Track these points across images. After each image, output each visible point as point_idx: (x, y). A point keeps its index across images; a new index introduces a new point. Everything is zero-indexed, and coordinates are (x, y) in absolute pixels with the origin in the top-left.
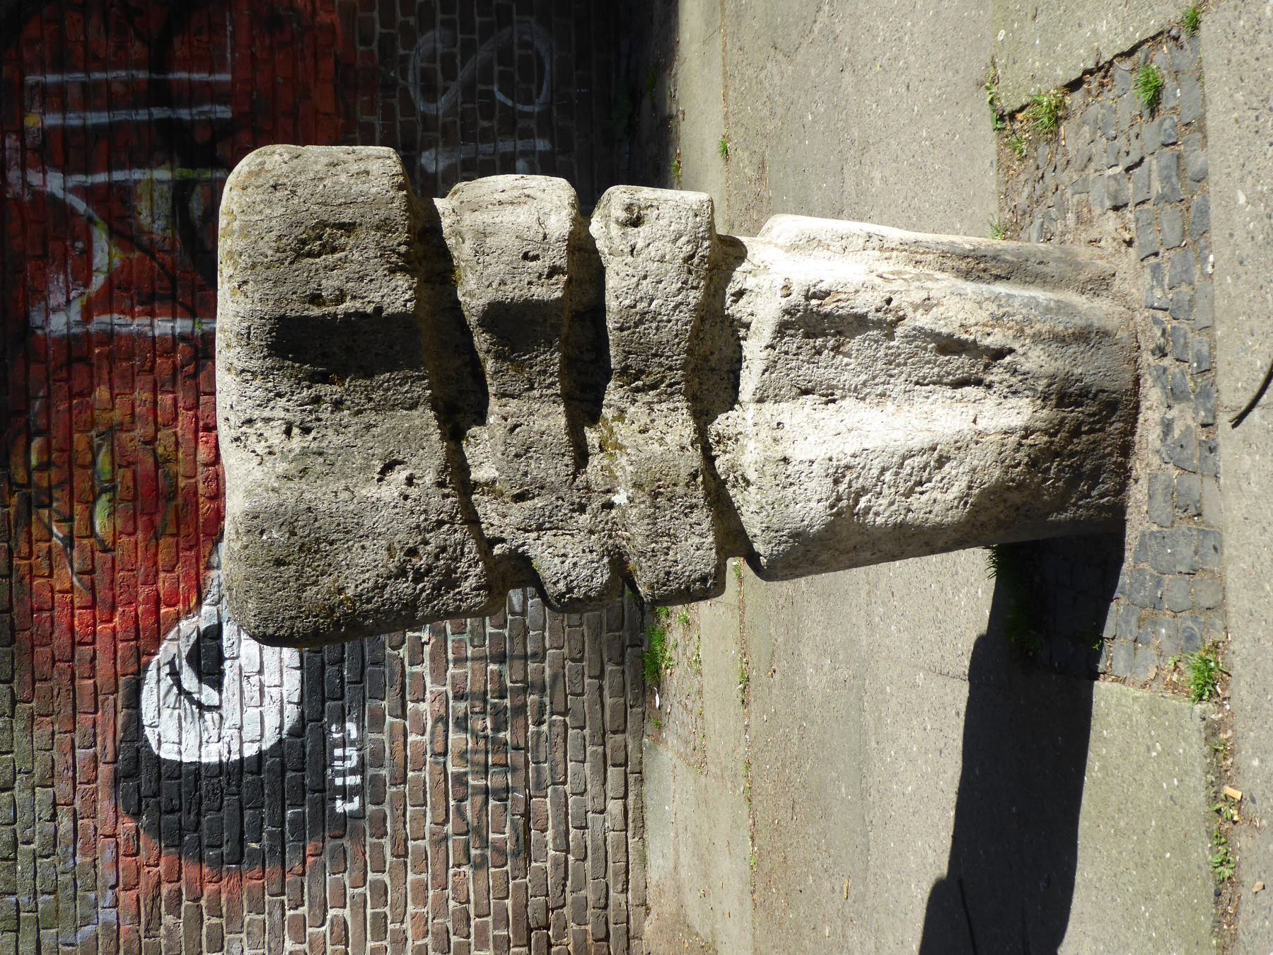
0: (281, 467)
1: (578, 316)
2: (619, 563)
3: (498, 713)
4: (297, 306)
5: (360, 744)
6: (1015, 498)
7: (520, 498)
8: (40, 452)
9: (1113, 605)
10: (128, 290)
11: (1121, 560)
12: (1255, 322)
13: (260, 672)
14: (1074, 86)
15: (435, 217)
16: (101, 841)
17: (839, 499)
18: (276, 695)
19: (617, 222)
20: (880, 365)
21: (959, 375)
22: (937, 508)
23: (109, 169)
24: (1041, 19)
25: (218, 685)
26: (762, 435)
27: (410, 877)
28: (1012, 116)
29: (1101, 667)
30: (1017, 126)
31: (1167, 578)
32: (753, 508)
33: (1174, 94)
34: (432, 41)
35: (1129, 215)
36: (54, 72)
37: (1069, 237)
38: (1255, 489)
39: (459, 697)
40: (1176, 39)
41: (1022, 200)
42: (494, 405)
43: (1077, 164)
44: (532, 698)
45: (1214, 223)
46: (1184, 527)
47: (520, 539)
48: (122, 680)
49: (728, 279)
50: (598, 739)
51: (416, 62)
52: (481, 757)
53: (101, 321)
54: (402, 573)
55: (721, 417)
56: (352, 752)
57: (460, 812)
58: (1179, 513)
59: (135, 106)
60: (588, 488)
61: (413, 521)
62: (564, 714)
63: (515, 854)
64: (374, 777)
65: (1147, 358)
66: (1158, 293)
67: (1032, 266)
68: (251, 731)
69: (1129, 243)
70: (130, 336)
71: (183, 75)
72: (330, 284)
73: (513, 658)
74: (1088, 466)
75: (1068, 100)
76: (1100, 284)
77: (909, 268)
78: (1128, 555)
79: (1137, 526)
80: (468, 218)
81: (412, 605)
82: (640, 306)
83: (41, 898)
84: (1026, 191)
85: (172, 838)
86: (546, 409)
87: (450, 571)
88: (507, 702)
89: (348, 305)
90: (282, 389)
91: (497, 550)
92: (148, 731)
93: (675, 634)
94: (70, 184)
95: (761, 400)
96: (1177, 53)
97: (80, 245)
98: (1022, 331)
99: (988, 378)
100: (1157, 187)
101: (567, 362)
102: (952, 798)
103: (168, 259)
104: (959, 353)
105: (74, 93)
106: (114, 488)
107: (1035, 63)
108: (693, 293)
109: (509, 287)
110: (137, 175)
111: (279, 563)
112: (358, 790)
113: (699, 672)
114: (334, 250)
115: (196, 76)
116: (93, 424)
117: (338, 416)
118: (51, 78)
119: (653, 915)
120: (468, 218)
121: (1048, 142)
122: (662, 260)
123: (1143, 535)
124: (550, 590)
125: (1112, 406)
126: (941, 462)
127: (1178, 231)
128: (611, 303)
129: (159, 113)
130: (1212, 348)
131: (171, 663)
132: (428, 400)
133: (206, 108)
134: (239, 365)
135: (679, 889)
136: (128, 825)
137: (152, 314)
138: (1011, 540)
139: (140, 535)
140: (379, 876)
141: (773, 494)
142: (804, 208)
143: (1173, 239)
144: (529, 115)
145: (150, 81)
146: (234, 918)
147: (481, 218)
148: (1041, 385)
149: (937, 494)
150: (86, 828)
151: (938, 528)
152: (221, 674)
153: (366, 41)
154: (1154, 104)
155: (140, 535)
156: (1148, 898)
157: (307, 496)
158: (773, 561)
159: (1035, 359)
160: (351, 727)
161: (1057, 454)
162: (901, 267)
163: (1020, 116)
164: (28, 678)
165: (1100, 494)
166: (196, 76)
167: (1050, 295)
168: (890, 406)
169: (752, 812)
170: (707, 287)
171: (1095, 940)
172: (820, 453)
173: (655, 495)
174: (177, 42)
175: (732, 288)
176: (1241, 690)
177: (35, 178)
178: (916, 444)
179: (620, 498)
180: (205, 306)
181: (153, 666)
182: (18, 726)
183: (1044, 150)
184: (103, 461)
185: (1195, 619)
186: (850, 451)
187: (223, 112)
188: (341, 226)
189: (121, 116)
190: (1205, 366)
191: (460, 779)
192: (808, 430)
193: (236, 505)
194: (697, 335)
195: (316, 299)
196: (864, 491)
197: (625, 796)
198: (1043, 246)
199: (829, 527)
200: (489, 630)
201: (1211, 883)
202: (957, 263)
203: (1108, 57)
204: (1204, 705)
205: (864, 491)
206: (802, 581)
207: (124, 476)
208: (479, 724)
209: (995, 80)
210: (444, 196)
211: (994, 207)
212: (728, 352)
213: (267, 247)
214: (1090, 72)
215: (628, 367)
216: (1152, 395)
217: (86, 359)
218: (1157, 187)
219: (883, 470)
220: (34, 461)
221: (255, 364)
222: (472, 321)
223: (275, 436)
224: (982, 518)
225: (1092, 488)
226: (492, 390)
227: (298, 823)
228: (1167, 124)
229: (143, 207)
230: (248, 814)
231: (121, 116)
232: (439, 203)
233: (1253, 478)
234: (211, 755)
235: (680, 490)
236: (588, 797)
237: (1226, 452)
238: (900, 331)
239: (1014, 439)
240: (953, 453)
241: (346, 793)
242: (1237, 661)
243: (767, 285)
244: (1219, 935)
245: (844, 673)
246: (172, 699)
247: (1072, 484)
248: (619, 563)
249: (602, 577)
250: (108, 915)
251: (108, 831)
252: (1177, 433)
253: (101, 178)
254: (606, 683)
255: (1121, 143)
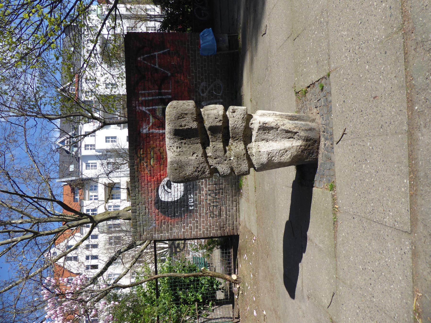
0: (176, 154)
1: (225, 128)
2: (232, 169)
3: (215, 193)
4: (178, 127)
5: (193, 198)
6: (299, 157)
7: (215, 158)
8: (142, 151)
9: (316, 175)
10: (155, 126)
11: (317, 167)
12: (340, 126)
13: (177, 187)
14: (308, 87)
15: (201, 112)
16: (153, 213)
17: (269, 158)
18: (180, 190)
20: (276, 135)
21: (289, 137)
22: (286, 159)
23: (152, 106)
24: (303, 76)
25: (171, 189)
26: (256, 147)
27: (202, 219)
28: (298, 93)
29: (314, 185)
30: (299, 94)
31: (325, 170)
32: (254, 160)
33: (326, 88)
34: (203, 84)
35: (318, 109)
36: (143, 91)
37: (308, 113)
38: (340, 155)
39: (209, 191)
40: (326, 78)
41: (300, 107)
42: (211, 143)
43: (309, 100)
44: (221, 191)
45: (333, 110)
46: (328, 161)
47: (216, 165)
48: (155, 188)
49: (250, 121)
50: (232, 197)
51: (201, 88)
52: (213, 200)
53: (151, 131)
54: (196, 171)
55: (249, 144)
56: (192, 199)
57: (210, 209)
58: (327, 159)
59: (156, 96)
60: (227, 157)
61: (198, 162)
62: (226, 193)
63: (219, 216)
64: (196, 203)
65: (321, 133)
66: (323, 122)
67: (302, 118)
68: (176, 196)
69: (318, 113)
70: (156, 133)
71: (163, 91)
72: (183, 124)
73: (218, 184)
74: (311, 151)
75: (307, 89)
76: (313, 121)
77: (281, 119)
78: (319, 167)
79: (320, 162)
80: (206, 112)
81: (198, 176)
82: (235, 126)
83: (144, 222)
84: (301, 105)
85: (164, 213)
86: (219, 144)
87: (204, 171)
88: (217, 191)
89: (186, 127)
90: (176, 141)
91: (212, 167)
92: (160, 196)
93: (244, 180)
94: (146, 109)
95: (256, 142)
96: (326, 81)
97: (148, 118)
98: (300, 129)
99: (294, 137)
100: (323, 104)
101: (223, 136)
102: (289, 207)
103: (162, 120)
104: (289, 133)
105: (147, 94)
106: (154, 157)
107: (302, 83)
108: (244, 124)
109: (213, 123)
110: (157, 107)
111: (176, 170)
112: (193, 205)
113: (248, 186)
114: (184, 118)
115: (166, 91)
116: (150, 147)
117: (185, 145)
118: (143, 92)
119: (241, 226)
120: (206, 112)
121: (304, 97)
122: (238, 118)
123: (321, 163)
124: (221, 174)
125: (315, 141)
126: (286, 151)
127: (327, 111)
128: (230, 126)
129: (160, 97)
130: (333, 131)
131: (163, 185)
132: (200, 142)
133: (167, 96)
134: (169, 137)
135: (245, 222)
136: (157, 211)
137: (159, 129)
138: (298, 164)
139: (158, 165)
140: (197, 219)
141: (258, 157)
142: (264, 109)
143: (326, 112)
144: (219, 96)
145: (158, 92)
146: (174, 225)
147: (208, 112)
148: (303, 138)
149: (286, 157)
150: (150, 211)
151: (286, 163)
152: (171, 187)
153: (193, 84)
154: (322, 90)
155: (158, 165)
156: (322, 224)
157: (180, 158)
158: (258, 168)
159: (302, 134)
160: (192, 195)
161: (306, 150)
162: (279, 119)
163: (299, 93)
164: (141, 187)
165: (313, 156)
166: (166, 91)
167: (305, 123)
168: (278, 142)
169: (257, 209)
170: (246, 123)
171: (313, 231)
172: (266, 150)
173: (238, 158)
174: (162, 85)
175: (250, 123)
176: (338, 189)
177: (141, 108)
178: (282, 148)
179: (232, 158)
180: (164, 128)
181: (160, 186)
182: (140, 195)
183: (304, 98)
184: (152, 153)
185: (330, 177)
186: (271, 150)
187: (170, 97)
188: (185, 114)
189: (154, 98)
190: (331, 134)
191: (209, 204)
192: (264, 146)
193: (169, 160)
194: (244, 131)
195: (181, 126)
196: (273, 156)
197: (236, 207)
198: (303, 114)
199: (267, 163)
200: (214, 180)
201: (333, 222)
202: (289, 118)
203: (314, 82)
204: (331, 192)
205: (273, 156)
206: (264, 171)
207: (155, 155)
208: (212, 195)
209: (295, 87)
210: (202, 108)
211: (295, 108)
212: (250, 133)
213: (173, 118)
214: (311, 85)
215: (233, 136)
216: (322, 139)
217: (149, 137)
218: (323, 104)
219: (276, 153)
220: (141, 153)
221: (171, 137)
222: (207, 129)
223: (175, 149)
224: (293, 161)
225: (312, 155)
226: (210, 141)
227: (184, 211)
228: (324, 93)
229: (158, 112)
230: (176, 209)
231: (154, 98)
232: (201, 110)
233: (340, 153)
234: (170, 200)
235: (242, 157)
236: (230, 207)
237: (335, 148)
238: (279, 129)
239: (299, 147)
240: (288, 150)
241: (191, 206)
242: (337, 184)
243: (256, 122)
244: (334, 230)
245: (271, 187)
246: (163, 191)
247: (309, 155)
248: (232, 169)
249: (229, 172)
250: (154, 225)
251: (154, 212)
252: (327, 146)
253: (151, 108)
254: (233, 188)
255: (317, 96)
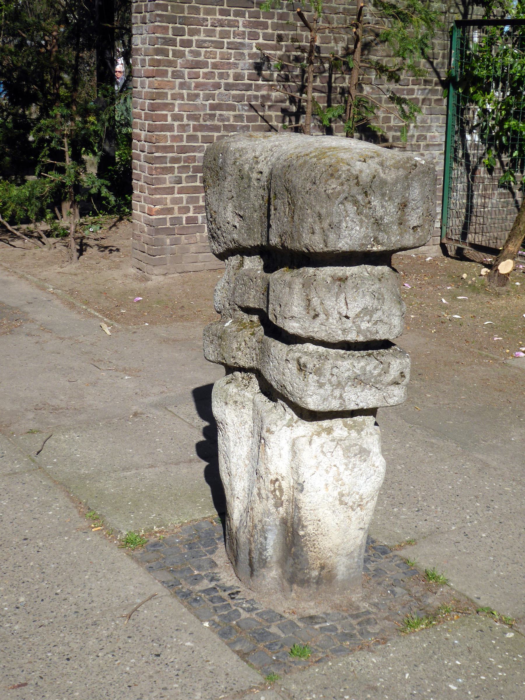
0: (247, 167)
19: (300, 357)
